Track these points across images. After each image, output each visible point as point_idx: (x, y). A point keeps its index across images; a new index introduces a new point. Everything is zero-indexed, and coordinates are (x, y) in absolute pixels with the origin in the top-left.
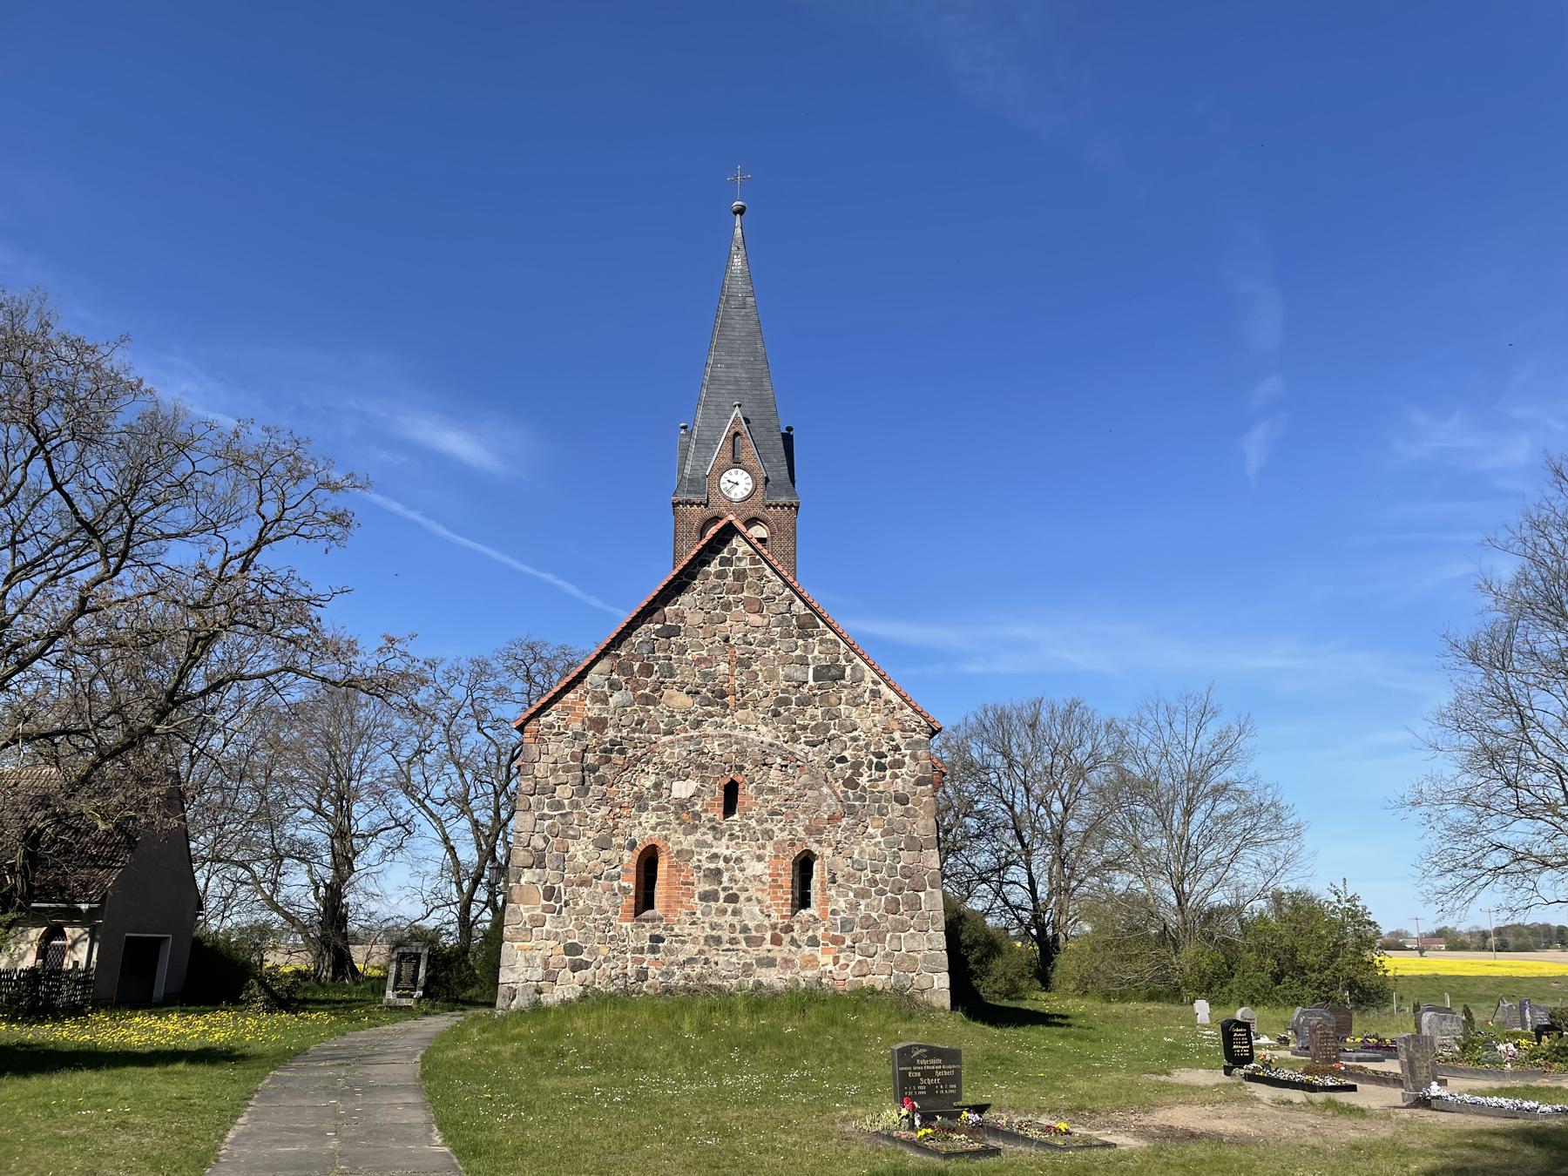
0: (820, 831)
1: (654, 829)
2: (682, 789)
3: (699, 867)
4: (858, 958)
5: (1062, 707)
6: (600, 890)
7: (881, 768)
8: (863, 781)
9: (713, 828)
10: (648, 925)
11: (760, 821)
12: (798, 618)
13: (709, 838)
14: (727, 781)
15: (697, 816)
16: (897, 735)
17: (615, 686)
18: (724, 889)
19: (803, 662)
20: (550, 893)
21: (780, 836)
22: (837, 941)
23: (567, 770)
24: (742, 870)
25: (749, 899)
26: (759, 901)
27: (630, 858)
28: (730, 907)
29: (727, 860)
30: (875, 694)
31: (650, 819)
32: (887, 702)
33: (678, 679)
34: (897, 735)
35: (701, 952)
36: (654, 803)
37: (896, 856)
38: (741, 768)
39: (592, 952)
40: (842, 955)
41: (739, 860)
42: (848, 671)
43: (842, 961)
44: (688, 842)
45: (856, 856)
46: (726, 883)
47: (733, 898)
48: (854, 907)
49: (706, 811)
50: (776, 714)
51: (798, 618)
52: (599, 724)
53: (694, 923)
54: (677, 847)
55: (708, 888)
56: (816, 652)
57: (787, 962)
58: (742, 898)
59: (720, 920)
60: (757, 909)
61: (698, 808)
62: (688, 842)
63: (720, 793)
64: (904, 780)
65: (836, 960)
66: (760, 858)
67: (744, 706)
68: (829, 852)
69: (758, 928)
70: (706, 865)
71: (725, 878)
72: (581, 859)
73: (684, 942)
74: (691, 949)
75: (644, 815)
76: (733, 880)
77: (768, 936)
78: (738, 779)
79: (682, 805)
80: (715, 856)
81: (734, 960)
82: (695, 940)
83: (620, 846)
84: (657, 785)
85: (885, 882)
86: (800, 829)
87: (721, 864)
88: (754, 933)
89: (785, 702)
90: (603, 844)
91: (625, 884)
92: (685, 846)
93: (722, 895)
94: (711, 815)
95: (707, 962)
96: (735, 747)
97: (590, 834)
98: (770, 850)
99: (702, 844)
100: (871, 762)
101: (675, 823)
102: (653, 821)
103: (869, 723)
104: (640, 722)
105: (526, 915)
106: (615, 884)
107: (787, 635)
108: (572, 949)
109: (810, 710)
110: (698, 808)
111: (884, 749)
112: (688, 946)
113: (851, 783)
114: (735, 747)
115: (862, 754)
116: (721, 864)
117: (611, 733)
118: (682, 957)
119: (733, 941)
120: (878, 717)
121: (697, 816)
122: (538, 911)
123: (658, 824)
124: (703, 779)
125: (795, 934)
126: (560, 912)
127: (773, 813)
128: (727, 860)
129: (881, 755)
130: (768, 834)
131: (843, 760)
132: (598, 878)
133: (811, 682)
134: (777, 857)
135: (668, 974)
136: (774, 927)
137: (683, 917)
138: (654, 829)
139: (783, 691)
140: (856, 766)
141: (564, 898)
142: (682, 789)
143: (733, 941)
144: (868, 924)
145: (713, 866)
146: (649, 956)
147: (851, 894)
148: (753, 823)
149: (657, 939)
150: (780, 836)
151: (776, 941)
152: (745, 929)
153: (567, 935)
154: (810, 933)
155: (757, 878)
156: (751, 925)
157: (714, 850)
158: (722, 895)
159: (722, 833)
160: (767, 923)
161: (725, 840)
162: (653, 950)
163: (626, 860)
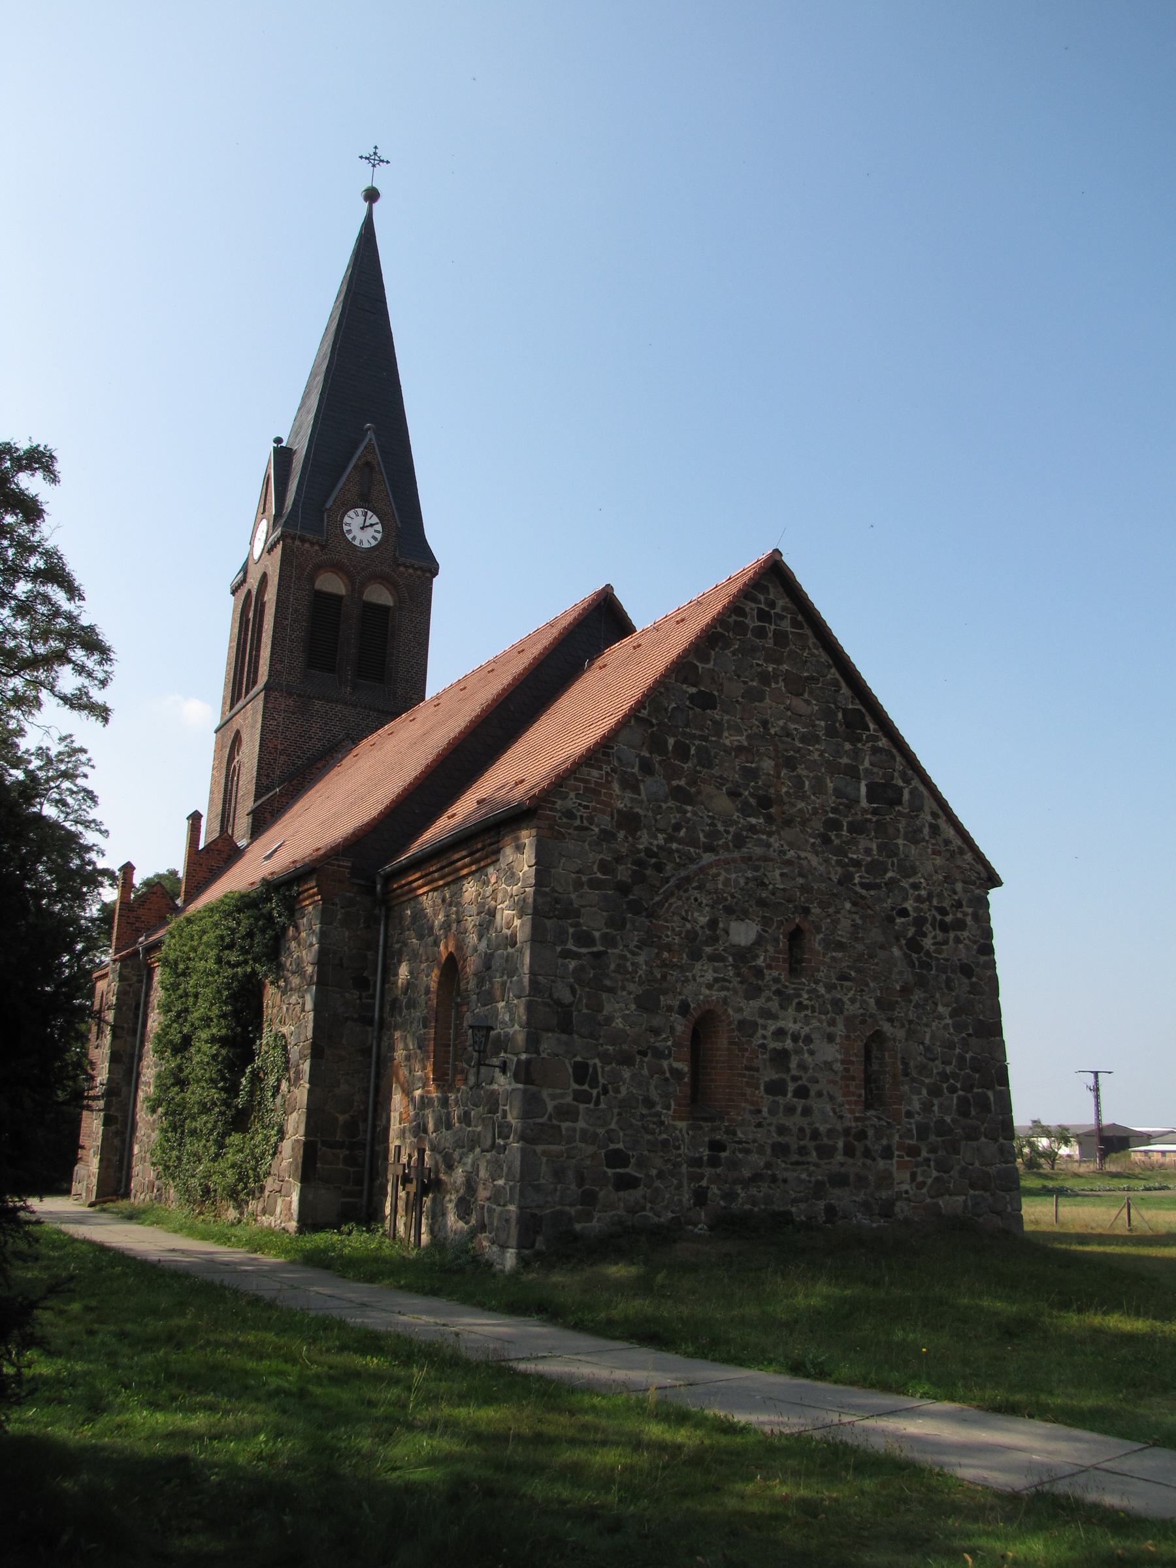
0: (891, 1006)
1: (710, 987)
2: (743, 933)
3: (763, 1046)
4: (935, 1174)
5: (76, 745)
6: (645, 1072)
7: (944, 928)
8: (928, 943)
9: (778, 992)
10: (707, 1126)
11: (830, 988)
12: (845, 711)
13: (774, 1006)
14: (792, 927)
15: (759, 972)
16: (959, 886)
17: (647, 767)
18: (795, 1079)
19: (852, 772)
20: (582, 1072)
21: (851, 1009)
22: (913, 1151)
23: (594, 884)
24: (812, 1053)
25: (820, 1094)
26: (831, 1098)
27: (681, 1026)
28: (800, 1104)
29: (795, 1038)
30: (935, 830)
31: (705, 972)
32: (947, 842)
33: (716, 771)
34: (959, 886)
35: (768, 1165)
36: (708, 950)
37: (965, 1043)
38: (806, 911)
39: (642, 1164)
40: (919, 1170)
41: (808, 1039)
42: (906, 796)
43: (920, 1179)
44: (750, 1008)
45: (927, 1042)
46: (794, 1072)
47: (802, 1092)
48: (927, 1108)
49: (769, 967)
50: (826, 840)
51: (845, 711)
52: (630, 821)
53: (759, 1125)
54: (738, 1016)
55: (775, 1077)
56: (867, 764)
57: (861, 1180)
58: (812, 1093)
59: (788, 1122)
60: (828, 1108)
61: (760, 962)
62: (750, 1008)
63: (783, 943)
64: (967, 948)
65: (913, 1176)
66: (831, 1038)
67: (788, 823)
68: (901, 1034)
69: (831, 1133)
70: (773, 1045)
71: (793, 1065)
72: (618, 1023)
73: (747, 1151)
74: (757, 1160)
75: (698, 966)
76: (802, 1066)
77: (840, 1144)
78: (805, 926)
79: (742, 955)
80: (780, 1033)
81: (804, 1176)
82: (761, 1150)
83: (670, 1009)
84: (713, 924)
85: (954, 1076)
86: (872, 1001)
87: (789, 1044)
88: (826, 1141)
89: (834, 825)
90: (648, 1003)
91: (676, 1065)
92: (746, 1015)
93: (791, 1087)
94: (775, 973)
95: (774, 1179)
96: (800, 881)
97: (632, 987)
98: (840, 1030)
99: (767, 1014)
100: (934, 918)
101: (735, 982)
102: (710, 976)
103: (930, 868)
104: (677, 828)
105: (550, 1105)
106: (665, 1064)
107: (831, 732)
108: (617, 1158)
109: (863, 843)
110: (760, 962)
111: (946, 904)
112: (754, 1157)
113: (914, 945)
114: (800, 881)
115: (925, 906)
116: (789, 1044)
117: (644, 840)
118: (747, 1173)
119: (802, 1151)
120: (939, 861)
121: (759, 972)
122: (569, 1099)
123: (716, 980)
124: (766, 922)
125: (869, 1143)
126: (597, 1103)
127: (843, 977)
128: (795, 1038)
129: (943, 911)
130: (838, 1005)
131: (904, 913)
132: (643, 1053)
133: (864, 803)
134: (847, 1037)
135: (730, 1196)
136: (847, 1132)
137: (748, 1116)
138: (710, 987)
139: (834, 810)
140: (919, 922)
141: (602, 1081)
142: (743, 933)
143: (802, 1151)
144: (942, 1129)
145: (778, 1045)
146: (708, 1171)
147: (924, 1091)
148: (822, 990)
149: (716, 1146)
150: (851, 1009)
151: (849, 1151)
152: (815, 1135)
153: (610, 1137)
154: (885, 1142)
155: (828, 1065)
156: (822, 1128)
157: (781, 1024)
158: (791, 1087)
159: (789, 998)
160: (839, 1127)
161: (791, 1011)
162: (714, 1162)
163: (679, 1029)
